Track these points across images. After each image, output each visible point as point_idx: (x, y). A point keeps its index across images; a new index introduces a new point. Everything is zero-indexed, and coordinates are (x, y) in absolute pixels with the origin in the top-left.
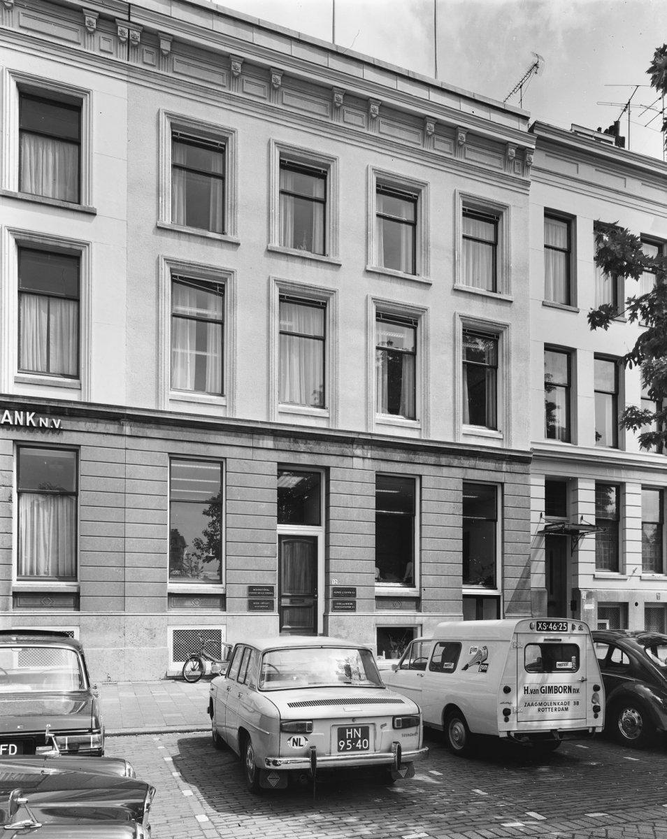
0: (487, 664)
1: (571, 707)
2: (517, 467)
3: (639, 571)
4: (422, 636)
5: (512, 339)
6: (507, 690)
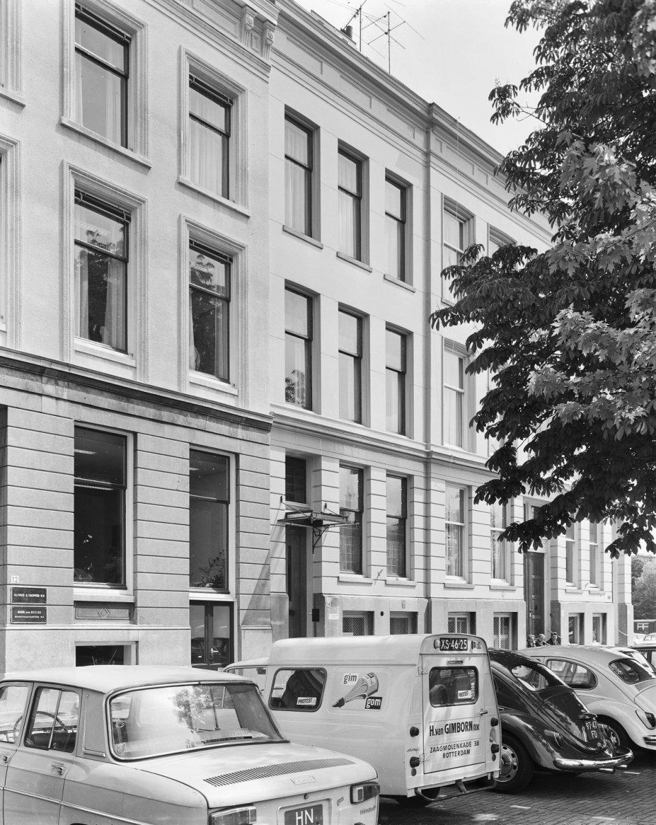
0: (381, 698)
1: (473, 749)
2: (255, 435)
3: (384, 575)
4: (240, 659)
5: (248, 264)
6: (414, 732)
